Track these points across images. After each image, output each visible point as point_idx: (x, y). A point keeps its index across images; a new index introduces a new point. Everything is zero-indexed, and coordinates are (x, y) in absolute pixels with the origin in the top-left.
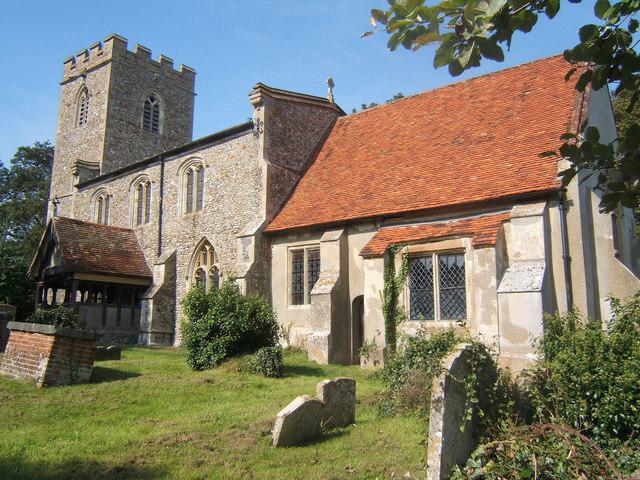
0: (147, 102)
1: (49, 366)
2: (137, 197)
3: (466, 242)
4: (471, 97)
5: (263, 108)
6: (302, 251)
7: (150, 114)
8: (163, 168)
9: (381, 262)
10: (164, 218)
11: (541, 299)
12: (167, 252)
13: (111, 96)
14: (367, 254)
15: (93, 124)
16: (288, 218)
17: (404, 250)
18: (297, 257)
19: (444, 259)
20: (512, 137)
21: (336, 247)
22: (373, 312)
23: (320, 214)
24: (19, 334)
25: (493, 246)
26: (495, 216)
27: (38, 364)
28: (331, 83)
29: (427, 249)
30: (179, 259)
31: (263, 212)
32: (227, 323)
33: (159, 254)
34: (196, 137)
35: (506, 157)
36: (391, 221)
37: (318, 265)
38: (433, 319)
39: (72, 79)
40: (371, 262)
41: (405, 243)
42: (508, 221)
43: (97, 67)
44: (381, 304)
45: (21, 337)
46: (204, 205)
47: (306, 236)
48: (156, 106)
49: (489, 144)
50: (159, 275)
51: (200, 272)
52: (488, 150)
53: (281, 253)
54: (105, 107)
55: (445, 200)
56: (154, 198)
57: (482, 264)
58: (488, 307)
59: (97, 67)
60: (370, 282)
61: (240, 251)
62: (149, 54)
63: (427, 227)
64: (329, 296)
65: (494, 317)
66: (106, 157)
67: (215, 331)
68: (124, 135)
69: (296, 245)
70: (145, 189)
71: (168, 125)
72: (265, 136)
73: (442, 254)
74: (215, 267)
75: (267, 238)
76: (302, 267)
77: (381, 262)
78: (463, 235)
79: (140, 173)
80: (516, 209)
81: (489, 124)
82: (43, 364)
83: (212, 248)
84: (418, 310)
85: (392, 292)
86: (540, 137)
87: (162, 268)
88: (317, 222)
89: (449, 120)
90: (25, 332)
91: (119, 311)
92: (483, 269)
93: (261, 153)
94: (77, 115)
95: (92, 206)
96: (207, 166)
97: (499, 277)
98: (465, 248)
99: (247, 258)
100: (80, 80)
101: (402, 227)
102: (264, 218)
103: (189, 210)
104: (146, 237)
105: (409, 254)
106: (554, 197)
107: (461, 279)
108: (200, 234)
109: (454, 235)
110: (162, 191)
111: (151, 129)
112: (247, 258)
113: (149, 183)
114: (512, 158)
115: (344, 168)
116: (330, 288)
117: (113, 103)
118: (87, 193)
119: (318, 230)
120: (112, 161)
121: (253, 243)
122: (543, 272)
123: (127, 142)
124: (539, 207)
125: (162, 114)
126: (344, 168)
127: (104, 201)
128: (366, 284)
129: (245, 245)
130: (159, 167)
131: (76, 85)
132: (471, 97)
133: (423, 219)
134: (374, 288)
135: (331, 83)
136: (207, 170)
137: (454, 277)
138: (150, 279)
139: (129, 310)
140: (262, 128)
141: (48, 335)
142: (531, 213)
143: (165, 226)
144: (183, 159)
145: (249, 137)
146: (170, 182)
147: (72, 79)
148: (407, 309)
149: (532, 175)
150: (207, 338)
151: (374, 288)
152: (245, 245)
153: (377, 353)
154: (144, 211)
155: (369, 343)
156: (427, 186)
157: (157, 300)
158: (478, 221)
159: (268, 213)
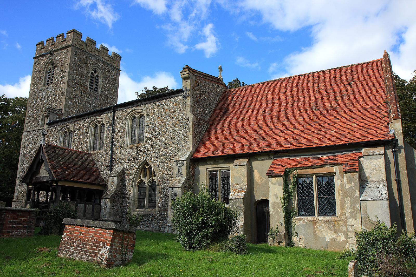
0: (92, 73)
1: (110, 252)
2: (93, 132)
3: (335, 169)
4: (315, 83)
5: (189, 81)
6: (217, 171)
7: (94, 81)
8: (114, 115)
9: (281, 179)
10: (115, 147)
11: (388, 205)
12: (118, 168)
13: (71, 68)
14: (271, 174)
15: (58, 85)
16: (207, 150)
17: (294, 172)
18: (213, 175)
19: (320, 179)
20: (350, 108)
21: (244, 170)
22: (276, 210)
23: (230, 148)
24: (75, 227)
25: (357, 172)
26: (352, 154)
27: (100, 250)
28: (221, 69)
29: (309, 173)
30: (126, 173)
31: (190, 146)
32: (212, 221)
33: (111, 170)
34: (121, 99)
35: (351, 119)
36: (279, 155)
37: (228, 181)
38: (314, 215)
39: (43, 55)
40: (274, 180)
41: (296, 168)
42: (362, 157)
43: (61, 49)
44: (282, 205)
45: (77, 230)
46: (145, 140)
47: (220, 162)
48: (97, 76)
49: (337, 112)
50: (113, 183)
51: (141, 182)
52: (338, 115)
53: (203, 170)
54: (67, 74)
55: (317, 143)
56: (106, 134)
57: (349, 182)
58: (353, 207)
59: (61, 49)
60: (274, 192)
61: (176, 170)
62: (94, 43)
63: (309, 160)
64: (242, 201)
65: (358, 215)
66: (66, 106)
67: (204, 224)
68: (78, 93)
69: (212, 167)
70: (99, 128)
71: (104, 89)
72: (191, 98)
73: (318, 175)
74: (153, 180)
75: (194, 162)
76: (216, 181)
77: (281, 179)
78: (335, 164)
79: (97, 117)
80: (364, 151)
81: (333, 99)
82: (105, 252)
83: (150, 167)
84: (303, 210)
85: (288, 198)
86: (370, 108)
87: (115, 179)
88: (229, 153)
89: (304, 95)
90: (81, 226)
91: (85, 206)
92: (350, 185)
93: (188, 109)
94: (45, 79)
95: (59, 137)
96: (148, 115)
97: (361, 193)
98: (335, 173)
99: (181, 175)
100: (49, 57)
101: (290, 159)
102: (191, 149)
103: (133, 141)
104: (101, 157)
105: (298, 175)
106: (390, 143)
107: (331, 191)
108: (142, 158)
109: (330, 164)
110: (113, 129)
111: (93, 90)
112: (181, 175)
113: (103, 124)
114: (355, 120)
115: (238, 121)
116: (242, 195)
117: (72, 72)
118: (55, 129)
119: (230, 158)
120: (70, 109)
121: (185, 165)
122: (386, 187)
123: (80, 97)
124: (381, 150)
125: (100, 82)
126: (238, 121)
127: (67, 135)
128: (270, 193)
129: (179, 166)
130: (112, 114)
131: (44, 60)
132: (315, 83)
133: (306, 154)
134: (276, 196)
135: (221, 69)
136: (147, 119)
137: (327, 189)
138: (105, 186)
139: (91, 206)
140: (189, 93)
141: (109, 229)
142: (377, 153)
143: (116, 152)
144: (129, 110)
145: (179, 98)
146: (120, 124)
147: (43, 55)
148: (296, 210)
149: (372, 131)
150: (199, 230)
151: (276, 196)
152: (179, 166)
153: (280, 236)
154: (98, 142)
155: (274, 229)
156: (302, 134)
157: (113, 200)
158: (341, 157)
159: (193, 146)
